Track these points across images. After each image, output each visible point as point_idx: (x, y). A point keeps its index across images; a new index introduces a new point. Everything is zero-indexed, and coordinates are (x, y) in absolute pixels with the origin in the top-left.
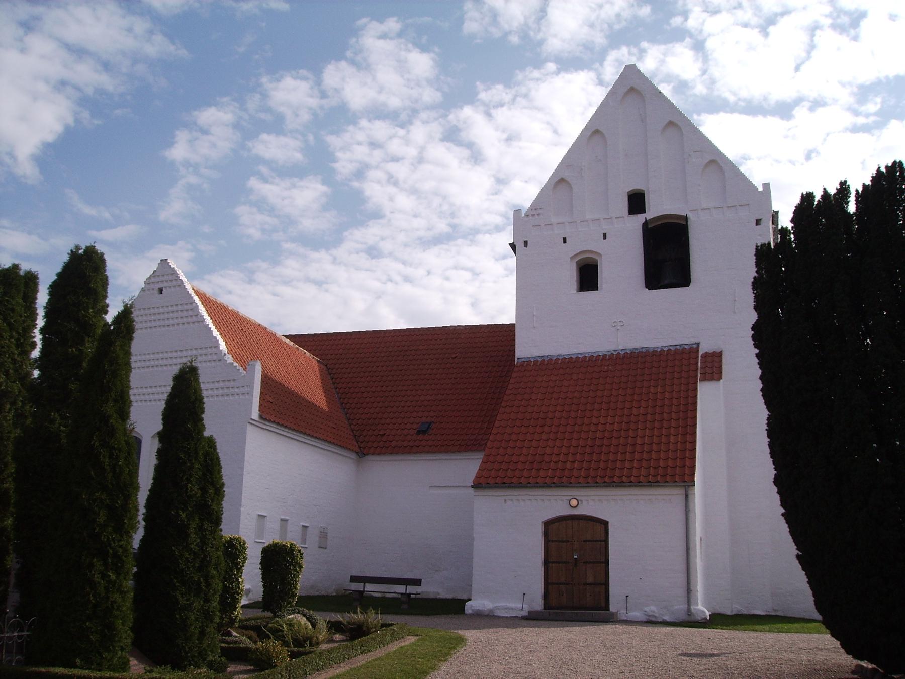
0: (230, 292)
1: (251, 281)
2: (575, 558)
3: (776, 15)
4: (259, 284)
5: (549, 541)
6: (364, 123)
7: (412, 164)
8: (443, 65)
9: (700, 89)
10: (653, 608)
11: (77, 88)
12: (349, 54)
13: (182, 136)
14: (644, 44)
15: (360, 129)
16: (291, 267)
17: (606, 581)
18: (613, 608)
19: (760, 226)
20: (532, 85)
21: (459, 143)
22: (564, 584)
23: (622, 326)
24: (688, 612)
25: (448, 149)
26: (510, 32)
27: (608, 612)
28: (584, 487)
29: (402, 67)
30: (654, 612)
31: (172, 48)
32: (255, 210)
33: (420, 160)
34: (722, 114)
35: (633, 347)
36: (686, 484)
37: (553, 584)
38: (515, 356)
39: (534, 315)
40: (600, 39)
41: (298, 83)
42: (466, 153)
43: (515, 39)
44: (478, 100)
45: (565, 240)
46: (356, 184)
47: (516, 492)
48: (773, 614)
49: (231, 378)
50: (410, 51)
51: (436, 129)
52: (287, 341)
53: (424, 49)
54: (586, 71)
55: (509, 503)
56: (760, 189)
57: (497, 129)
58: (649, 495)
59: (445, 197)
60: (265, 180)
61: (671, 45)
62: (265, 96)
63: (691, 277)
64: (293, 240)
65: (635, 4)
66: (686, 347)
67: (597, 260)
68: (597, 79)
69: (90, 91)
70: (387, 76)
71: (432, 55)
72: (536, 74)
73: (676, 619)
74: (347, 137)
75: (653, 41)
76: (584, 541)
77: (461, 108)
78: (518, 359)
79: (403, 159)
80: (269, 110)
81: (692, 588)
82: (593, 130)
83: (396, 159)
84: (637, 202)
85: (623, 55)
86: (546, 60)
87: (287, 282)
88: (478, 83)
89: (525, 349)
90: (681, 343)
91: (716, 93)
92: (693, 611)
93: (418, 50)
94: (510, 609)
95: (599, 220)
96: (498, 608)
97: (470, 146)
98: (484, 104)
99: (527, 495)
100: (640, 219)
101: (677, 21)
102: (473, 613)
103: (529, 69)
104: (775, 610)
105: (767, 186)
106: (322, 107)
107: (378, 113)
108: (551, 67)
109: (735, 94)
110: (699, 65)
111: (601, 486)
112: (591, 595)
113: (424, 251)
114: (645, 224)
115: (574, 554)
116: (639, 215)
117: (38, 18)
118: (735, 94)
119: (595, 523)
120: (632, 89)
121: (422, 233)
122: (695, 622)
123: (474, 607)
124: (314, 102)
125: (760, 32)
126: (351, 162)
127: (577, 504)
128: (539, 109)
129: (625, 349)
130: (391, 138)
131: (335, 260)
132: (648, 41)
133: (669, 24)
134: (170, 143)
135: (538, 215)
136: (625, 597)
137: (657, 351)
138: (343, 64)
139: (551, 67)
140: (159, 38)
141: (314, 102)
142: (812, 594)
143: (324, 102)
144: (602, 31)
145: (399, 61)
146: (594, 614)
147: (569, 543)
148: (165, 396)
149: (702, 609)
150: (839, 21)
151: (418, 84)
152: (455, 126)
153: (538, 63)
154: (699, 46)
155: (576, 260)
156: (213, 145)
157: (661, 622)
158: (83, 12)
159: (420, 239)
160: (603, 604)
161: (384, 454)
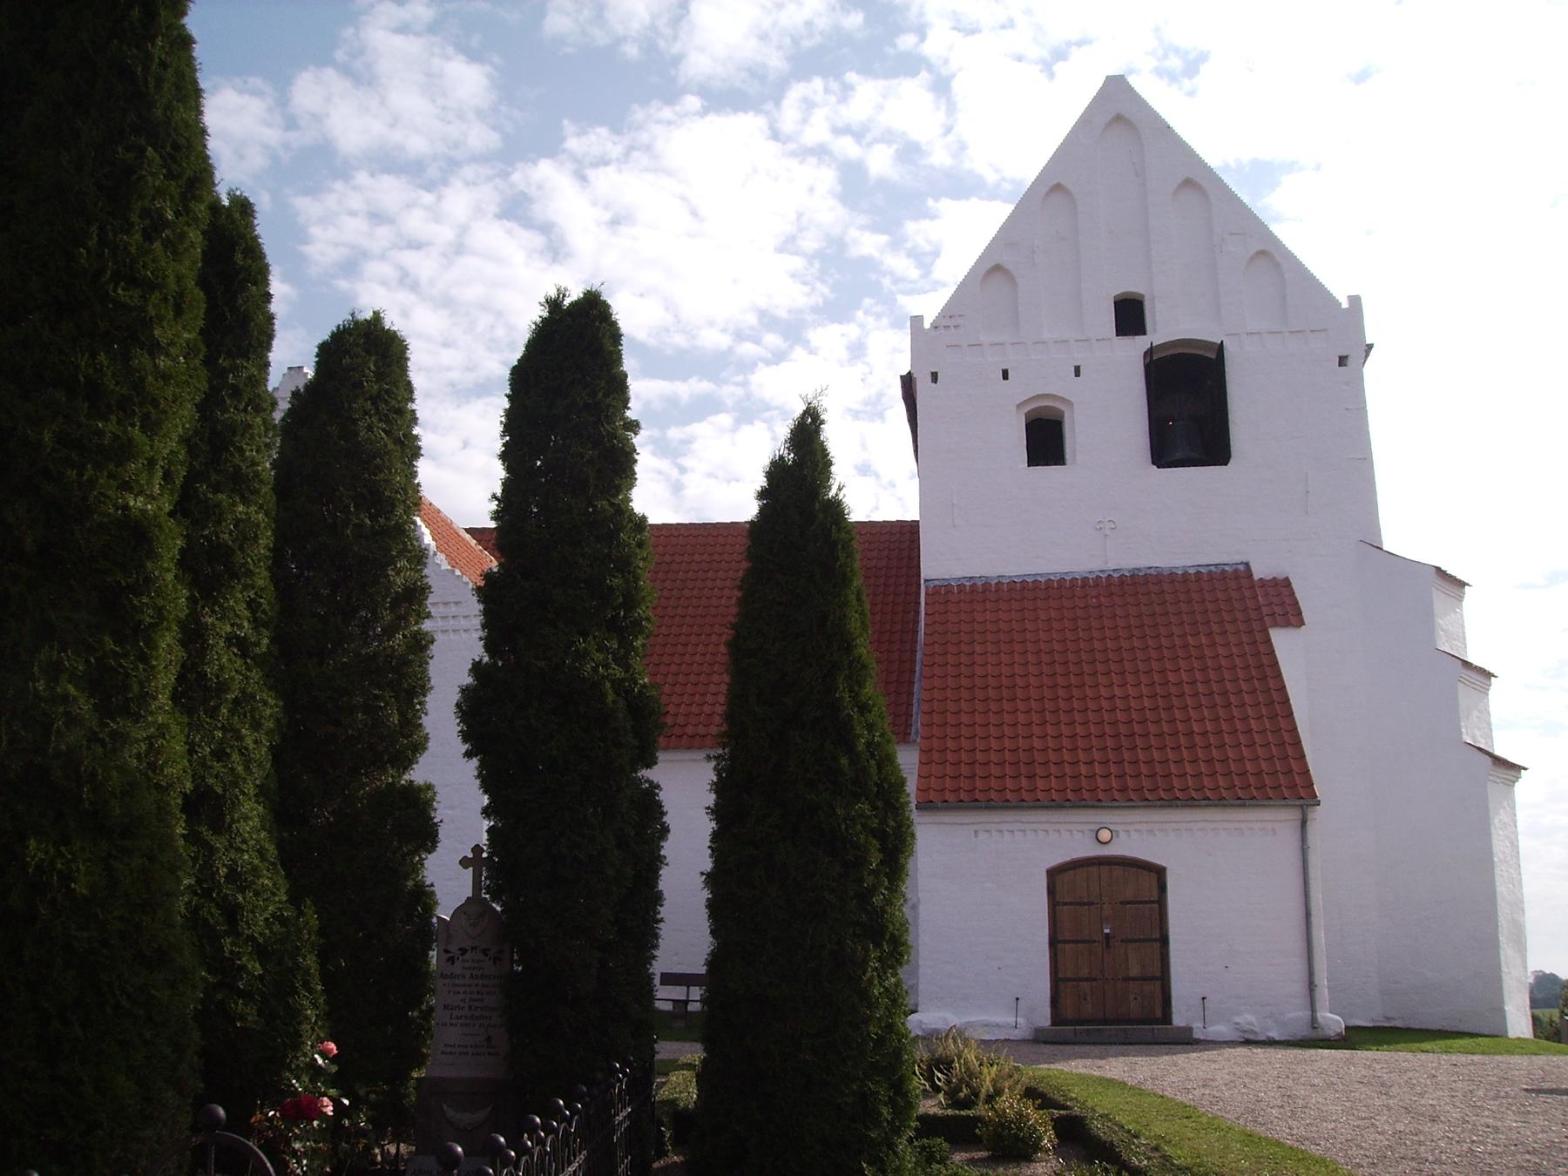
2: (1106, 934)
3: (1069, 44)
5: (1058, 903)
6: (362, 178)
7: (444, 255)
8: (507, 87)
9: (940, 157)
10: (1250, 1018)
12: (340, 55)
14: (851, 77)
15: (355, 188)
17: (1163, 972)
18: (1178, 1020)
19: (1345, 367)
20: (657, 129)
21: (528, 223)
22: (1087, 980)
23: (1112, 529)
24: (1312, 1024)
25: (509, 232)
26: (625, 39)
27: (1169, 1026)
28: (1124, 807)
29: (433, 85)
30: (1251, 1024)
33: (459, 249)
34: (974, 200)
35: (1134, 567)
36: (1302, 802)
37: (1068, 980)
38: (920, 576)
39: (953, 505)
40: (776, 62)
41: (245, 99)
42: (538, 240)
43: (632, 51)
44: (564, 151)
45: (1005, 375)
46: (343, 284)
47: (1009, 816)
48: (1386, 1025)
49: (452, 599)
50: (449, 59)
51: (488, 195)
52: (468, 537)
53: (474, 56)
54: (751, 114)
55: (983, 836)
56: (1345, 305)
57: (594, 203)
58: (1239, 821)
59: (499, 314)
61: (895, 82)
63: (1232, 449)
65: (838, 6)
66: (1227, 568)
67: (1063, 412)
68: (769, 128)
70: (407, 99)
71: (488, 69)
72: (667, 113)
73: (1292, 1036)
74: (330, 201)
75: (867, 71)
76: (1122, 903)
77: (535, 163)
78: (926, 581)
79: (429, 244)
81: (1316, 982)
82: (1051, 185)
83: (416, 245)
84: (1130, 316)
85: (815, 92)
86: (684, 91)
88: (566, 122)
90: (1217, 562)
91: (967, 165)
92: (1320, 1020)
93: (462, 58)
94: (994, 1026)
95: (1002, 344)
96: (970, 1024)
97: (546, 228)
98: (576, 160)
99: (1016, 822)
100: (1140, 344)
101: (907, 41)
102: (924, 1034)
103: (655, 103)
104: (1388, 1019)
105: (1355, 301)
106: (286, 146)
107: (388, 162)
108: (692, 102)
109: (997, 171)
110: (941, 116)
111: (1155, 806)
112: (1136, 999)
113: (459, 406)
114: (1149, 353)
115: (1104, 926)
116: (1137, 337)
118: (997, 171)
119: (1140, 870)
120: (1119, 119)
121: (455, 375)
122: (1323, 1040)
123: (925, 1024)
124: (273, 136)
125: (1041, 71)
126: (336, 245)
127: (1110, 837)
128: (668, 173)
129: (1120, 570)
130: (409, 206)
132: (859, 72)
133: (894, 46)
135: (955, 327)
136: (1015, 1000)
137: (1177, 574)
138: (329, 73)
139: (692, 102)
141: (273, 136)
143: (292, 136)
144: (780, 47)
145: (428, 75)
146: (1156, 1032)
147: (1093, 907)
149: (1333, 1022)
150: (1167, 63)
151: (461, 116)
152: (522, 193)
153: (671, 94)
154: (941, 87)
155: (1026, 411)
157: (1264, 1041)
159: (452, 385)
160: (1159, 1014)
161: (676, 748)
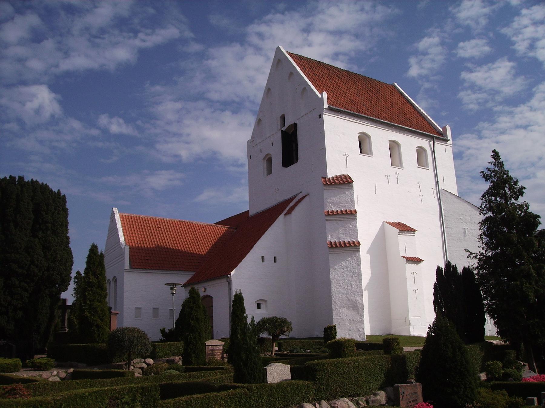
0: (469, 148)
1: (480, 138)
4: (486, 138)
6: (524, 11)
11: (345, 54)
13: (413, 61)
16: (504, 121)
31: (389, 11)
32: (469, 92)
46: (531, 54)
60: (471, 71)
62: (454, 18)
64: (501, 103)
69: (353, 54)
74: (515, 25)
80: (458, 26)
87: (503, 132)
89: (251, 214)
117: (310, 24)
131: (532, 109)
134: (407, 67)
140: (380, 8)
142: (179, 313)
143: (494, 7)
148: (105, 266)
156: (433, 61)
158: (333, 10)
